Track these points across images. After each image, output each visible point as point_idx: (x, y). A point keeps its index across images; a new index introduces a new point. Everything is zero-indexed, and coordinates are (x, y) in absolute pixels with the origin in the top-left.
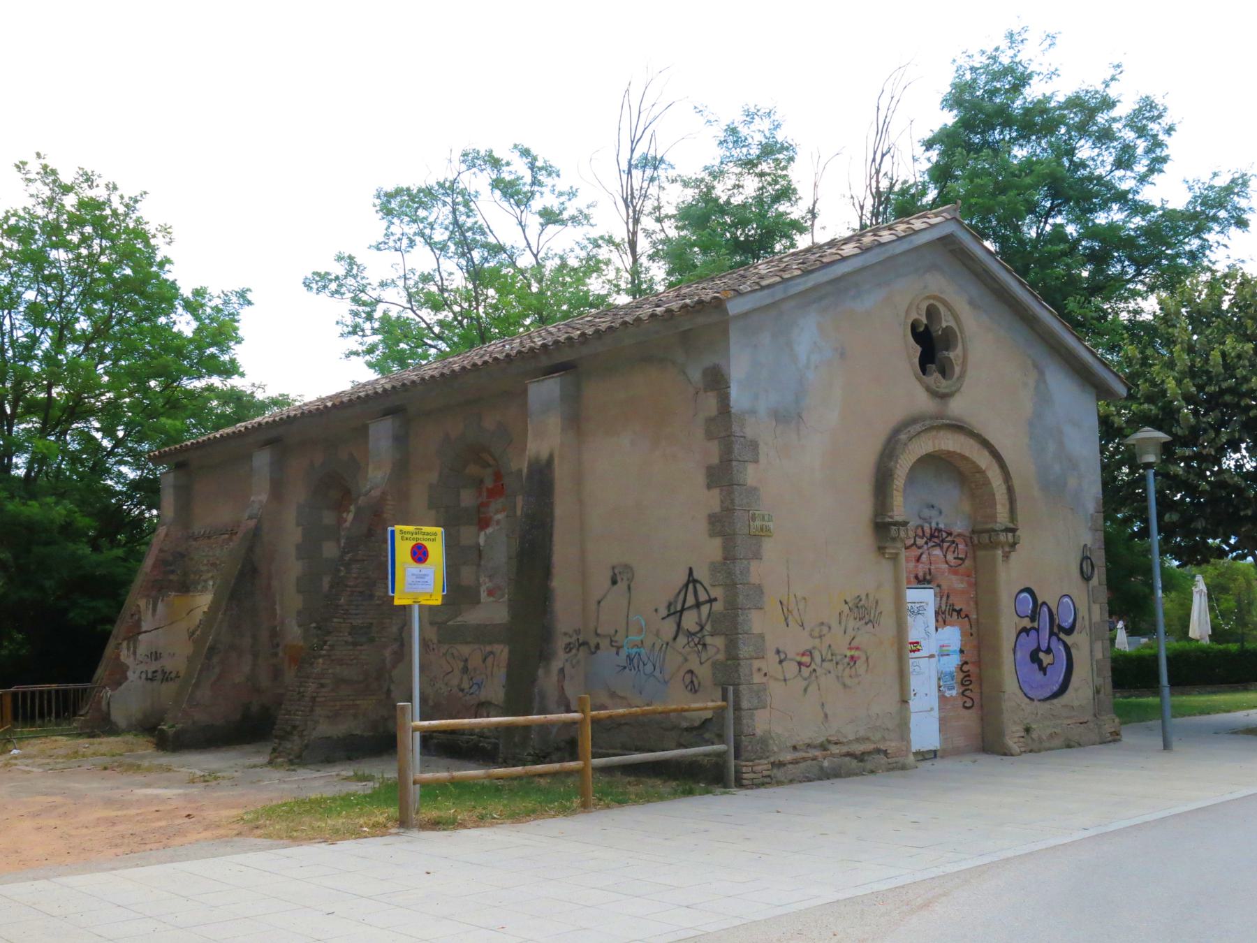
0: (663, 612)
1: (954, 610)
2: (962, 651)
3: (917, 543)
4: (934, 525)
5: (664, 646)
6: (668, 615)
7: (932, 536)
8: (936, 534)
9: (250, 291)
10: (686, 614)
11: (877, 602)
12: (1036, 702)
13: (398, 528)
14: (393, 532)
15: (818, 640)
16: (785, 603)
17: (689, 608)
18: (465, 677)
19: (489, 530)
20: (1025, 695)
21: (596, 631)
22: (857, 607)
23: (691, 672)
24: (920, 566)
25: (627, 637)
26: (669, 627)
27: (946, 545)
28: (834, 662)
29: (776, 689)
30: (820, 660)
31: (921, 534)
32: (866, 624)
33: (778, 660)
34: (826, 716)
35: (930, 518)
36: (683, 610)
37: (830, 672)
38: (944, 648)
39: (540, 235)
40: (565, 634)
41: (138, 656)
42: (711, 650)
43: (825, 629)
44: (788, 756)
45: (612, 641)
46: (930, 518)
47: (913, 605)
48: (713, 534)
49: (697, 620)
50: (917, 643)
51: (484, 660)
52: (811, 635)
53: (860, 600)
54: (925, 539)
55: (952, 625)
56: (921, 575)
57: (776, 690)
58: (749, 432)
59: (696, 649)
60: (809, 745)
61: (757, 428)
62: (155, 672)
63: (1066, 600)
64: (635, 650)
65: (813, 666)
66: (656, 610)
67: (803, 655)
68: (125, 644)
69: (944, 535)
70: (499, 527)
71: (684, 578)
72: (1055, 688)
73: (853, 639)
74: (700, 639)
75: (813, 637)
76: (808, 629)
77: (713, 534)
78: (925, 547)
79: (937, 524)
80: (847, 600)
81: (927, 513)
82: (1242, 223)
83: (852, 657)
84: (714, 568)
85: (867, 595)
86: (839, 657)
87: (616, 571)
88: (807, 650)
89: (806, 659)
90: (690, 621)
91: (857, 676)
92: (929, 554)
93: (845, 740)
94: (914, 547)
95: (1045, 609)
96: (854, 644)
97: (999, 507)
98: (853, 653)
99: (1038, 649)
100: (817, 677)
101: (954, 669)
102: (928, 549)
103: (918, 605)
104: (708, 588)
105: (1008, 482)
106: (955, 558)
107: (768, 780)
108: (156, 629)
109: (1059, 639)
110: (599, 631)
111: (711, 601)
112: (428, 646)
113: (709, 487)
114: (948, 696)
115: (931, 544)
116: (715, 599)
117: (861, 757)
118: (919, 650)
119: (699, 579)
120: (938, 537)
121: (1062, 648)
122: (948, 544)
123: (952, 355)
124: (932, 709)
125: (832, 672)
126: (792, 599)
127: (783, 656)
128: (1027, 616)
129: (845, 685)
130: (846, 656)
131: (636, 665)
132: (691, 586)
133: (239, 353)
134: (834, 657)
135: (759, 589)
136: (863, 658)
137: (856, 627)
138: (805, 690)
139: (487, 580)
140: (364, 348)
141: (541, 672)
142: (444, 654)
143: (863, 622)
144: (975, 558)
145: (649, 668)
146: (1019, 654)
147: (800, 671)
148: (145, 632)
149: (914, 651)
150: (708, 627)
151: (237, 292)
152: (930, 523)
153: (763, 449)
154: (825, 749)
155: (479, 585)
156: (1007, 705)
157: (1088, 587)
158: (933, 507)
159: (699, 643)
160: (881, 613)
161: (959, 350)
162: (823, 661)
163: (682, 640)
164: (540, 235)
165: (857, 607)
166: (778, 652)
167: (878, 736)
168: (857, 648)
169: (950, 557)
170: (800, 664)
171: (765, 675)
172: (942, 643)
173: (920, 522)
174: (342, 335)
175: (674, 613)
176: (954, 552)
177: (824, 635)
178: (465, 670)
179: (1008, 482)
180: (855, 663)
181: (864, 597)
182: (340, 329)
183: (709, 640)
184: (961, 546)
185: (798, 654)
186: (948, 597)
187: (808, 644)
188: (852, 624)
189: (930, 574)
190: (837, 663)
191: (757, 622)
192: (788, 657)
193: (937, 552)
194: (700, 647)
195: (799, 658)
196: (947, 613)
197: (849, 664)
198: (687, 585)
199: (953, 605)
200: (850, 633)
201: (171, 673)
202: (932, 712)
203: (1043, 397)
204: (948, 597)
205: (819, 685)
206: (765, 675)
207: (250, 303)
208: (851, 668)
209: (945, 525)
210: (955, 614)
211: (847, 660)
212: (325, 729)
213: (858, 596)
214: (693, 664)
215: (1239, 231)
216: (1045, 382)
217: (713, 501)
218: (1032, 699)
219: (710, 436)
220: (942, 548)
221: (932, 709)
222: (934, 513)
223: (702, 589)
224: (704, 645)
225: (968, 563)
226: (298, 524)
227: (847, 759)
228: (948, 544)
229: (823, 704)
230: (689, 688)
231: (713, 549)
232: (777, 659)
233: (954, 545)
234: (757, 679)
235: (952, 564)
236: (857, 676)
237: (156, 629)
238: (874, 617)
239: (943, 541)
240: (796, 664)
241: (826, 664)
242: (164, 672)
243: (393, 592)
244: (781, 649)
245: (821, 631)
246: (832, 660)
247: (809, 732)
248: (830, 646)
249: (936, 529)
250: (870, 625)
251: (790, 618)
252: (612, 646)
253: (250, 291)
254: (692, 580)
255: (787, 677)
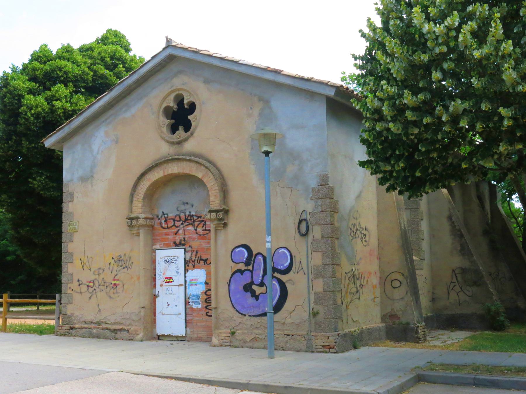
1: (201, 260)
3: (176, 224)
4: (187, 213)
7: (186, 220)
8: (189, 218)
11: (130, 258)
12: (247, 316)
15: (97, 276)
16: (82, 259)
20: (237, 311)
22: (119, 260)
24: (177, 236)
27: (196, 223)
28: (105, 286)
30: (98, 285)
31: (179, 220)
32: (124, 268)
33: (78, 284)
34: (100, 310)
35: (185, 210)
37: (103, 290)
38: (193, 281)
43: (101, 271)
46: (185, 210)
47: (168, 258)
50: (171, 278)
52: (94, 273)
53: (121, 257)
54: (181, 222)
55: (199, 268)
56: (178, 241)
57: (77, 297)
58: (70, 190)
60: (92, 322)
65: (94, 287)
67: (90, 282)
69: (195, 218)
73: (116, 276)
75: (95, 275)
76: (93, 270)
78: (182, 226)
79: (190, 212)
80: (114, 257)
81: (182, 208)
83: (115, 284)
85: (125, 254)
86: (107, 284)
88: (92, 280)
89: (91, 284)
91: (117, 293)
92: (184, 229)
93: (109, 322)
94: (174, 227)
95: (260, 258)
96: (116, 278)
98: (115, 282)
99: (252, 283)
100: (96, 292)
101: (200, 293)
102: (183, 227)
103: (172, 258)
106: (203, 230)
107: (67, 334)
114: (195, 308)
115: (185, 224)
117: (115, 331)
118: (171, 282)
120: (191, 220)
122: (198, 223)
124: (179, 314)
125: (104, 290)
126: (86, 258)
127: (81, 282)
128: (242, 262)
129: (110, 297)
130: (111, 284)
134: (105, 284)
135: (72, 255)
136: (121, 285)
137: (118, 270)
138: (90, 298)
143: (122, 267)
146: (233, 286)
147: (88, 289)
149: (168, 282)
152: (185, 213)
153: (76, 195)
157: (307, 242)
158: (187, 203)
160: (133, 263)
162: (99, 285)
165: (119, 260)
166: (79, 281)
167: (128, 322)
168: (118, 280)
169: (200, 229)
170: (88, 286)
171: (73, 290)
172: (191, 279)
173: (178, 213)
176: (203, 227)
177: (100, 274)
180: (116, 287)
181: (122, 256)
185: (87, 282)
186: (197, 252)
187: (93, 277)
188: (116, 268)
189: (184, 240)
190: (107, 287)
192: (83, 283)
193: (190, 228)
195: (88, 284)
196: (196, 261)
197: (113, 287)
199: (201, 257)
200: (115, 273)
202: (180, 316)
204: (197, 252)
205: (97, 296)
206: (73, 290)
208: (114, 289)
209: (196, 212)
210: (202, 262)
211: (112, 285)
213: (120, 255)
216: (270, 108)
220: (193, 226)
221: (179, 314)
222: (187, 207)
227: (106, 331)
228: (198, 223)
229: (98, 305)
232: (78, 283)
233: (203, 223)
235: (201, 234)
236: (117, 293)
238: (129, 265)
239: (194, 221)
240: (86, 286)
241: (101, 287)
244: (80, 279)
245: (99, 271)
246: (104, 285)
247: (90, 316)
248: (103, 279)
249: (189, 215)
250: (126, 269)
251: (85, 266)
255: (82, 291)
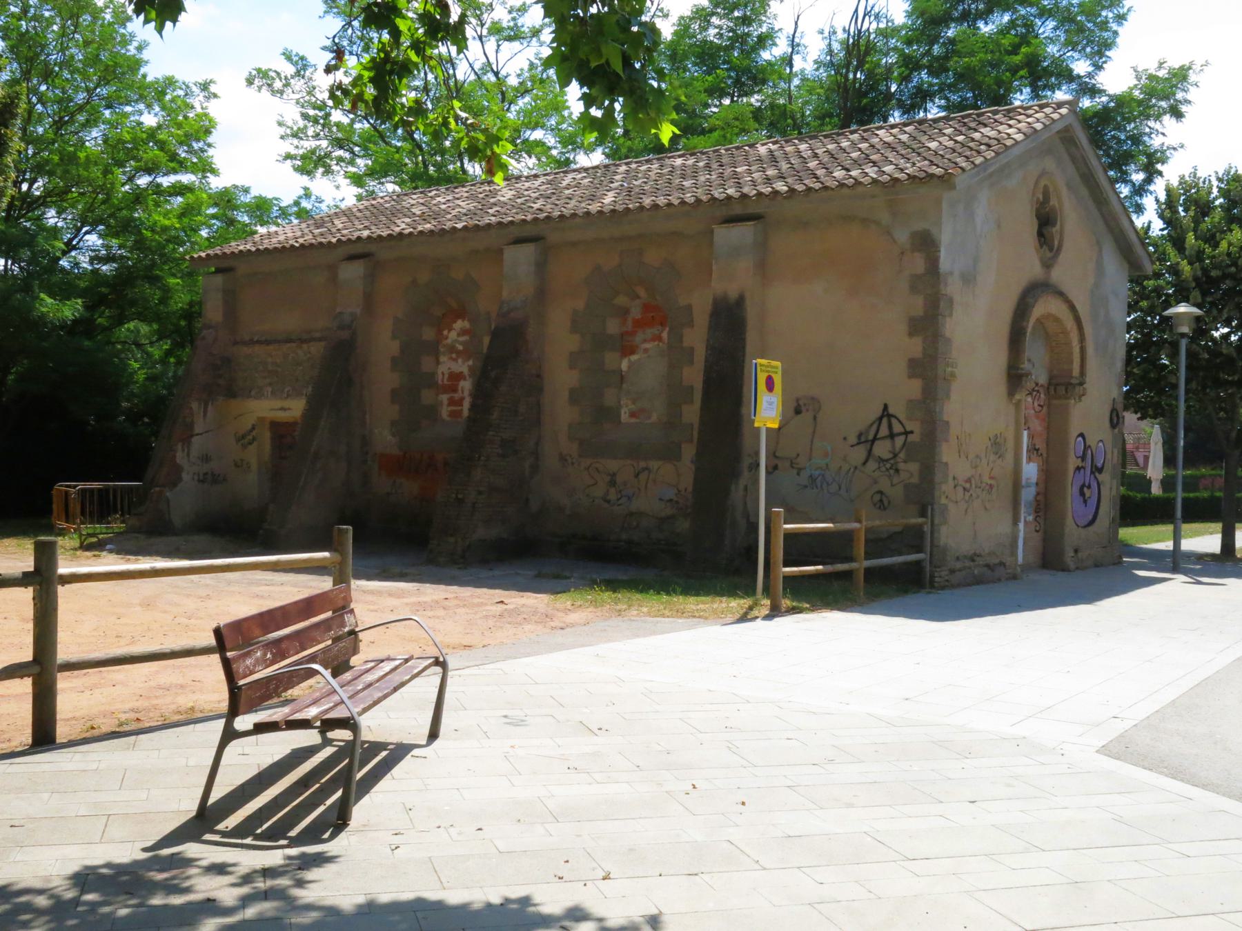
0: (853, 440)
2: (1037, 484)
5: (852, 470)
6: (858, 444)
9: (214, 82)
10: (877, 443)
13: (759, 361)
14: (756, 364)
17: (883, 438)
18: (613, 490)
19: (634, 358)
21: (774, 453)
23: (880, 492)
25: (810, 460)
26: (859, 454)
29: (951, 507)
36: (875, 439)
39: (497, 52)
40: (749, 455)
41: (191, 457)
42: (903, 475)
44: (958, 565)
45: (792, 463)
48: (912, 376)
49: (890, 449)
51: (637, 476)
55: (1034, 462)
59: (887, 473)
61: (953, 287)
62: (206, 474)
63: (1101, 444)
64: (817, 473)
66: (845, 439)
68: (179, 446)
70: (646, 355)
71: (879, 413)
72: (1090, 517)
74: (892, 465)
77: (912, 376)
82: (1177, 114)
84: (912, 404)
87: (801, 403)
90: (882, 449)
95: (1089, 452)
97: (1075, 363)
104: (904, 422)
105: (1082, 343)
108: (206, 432)
109: (1095, 477)
110: (777, 454)
111: (907, 433)
112: (566, 460)
113: (911, 334)
116: (912, 432)
119: (894, 414)
121: (1096, 485)
123: (1054, 230)
131: (819, 485)
132: (885, 421)
133: (218, 155)
139: (629, 402)
140: (301, 152)
141: (733, 487)
142: (587, 469)
144: (1049, 406)
145: (834, 488)
148: (197, 435)
150: (902, 455)
151: (200, 84)
154: (973, 560)
155: (619, 407)
156: (1067, 530)
159: (891, 468)
161: (1058, 226)
163: (872, 465)
164: (497, 52)
166: (954, 478)
174: (282, 137)
175: (866, 441)
178: (613, 483)
179: (1082, 343)
182: (282, 131)
183: (901, 466)
184: (1042, 396)
191: (947, 454)
194: (892, 472)
198: (881, 419)
201: (219, 475)
203: (1100, 270)
207: (215, 96)
212: (481, 533)
214: (884, 484)
215: (1174, 120)
217: (916, 347)
218: (1078, 526)
219: (914, 289)
223: (896, 421)
224: (897, 471)
225: (1045, 409)
226: (394, 337)
230: (878, 506)
231: (914, 388)
234: (943, 501)
237: (206, 432)
242: (213, 475)
243: (755, 416)
252: (793, 467)
253: (214, 82)
254: (886, 413)
